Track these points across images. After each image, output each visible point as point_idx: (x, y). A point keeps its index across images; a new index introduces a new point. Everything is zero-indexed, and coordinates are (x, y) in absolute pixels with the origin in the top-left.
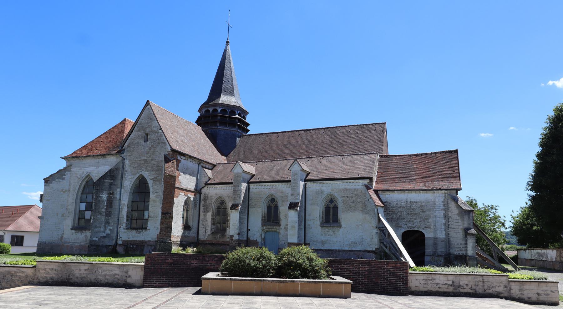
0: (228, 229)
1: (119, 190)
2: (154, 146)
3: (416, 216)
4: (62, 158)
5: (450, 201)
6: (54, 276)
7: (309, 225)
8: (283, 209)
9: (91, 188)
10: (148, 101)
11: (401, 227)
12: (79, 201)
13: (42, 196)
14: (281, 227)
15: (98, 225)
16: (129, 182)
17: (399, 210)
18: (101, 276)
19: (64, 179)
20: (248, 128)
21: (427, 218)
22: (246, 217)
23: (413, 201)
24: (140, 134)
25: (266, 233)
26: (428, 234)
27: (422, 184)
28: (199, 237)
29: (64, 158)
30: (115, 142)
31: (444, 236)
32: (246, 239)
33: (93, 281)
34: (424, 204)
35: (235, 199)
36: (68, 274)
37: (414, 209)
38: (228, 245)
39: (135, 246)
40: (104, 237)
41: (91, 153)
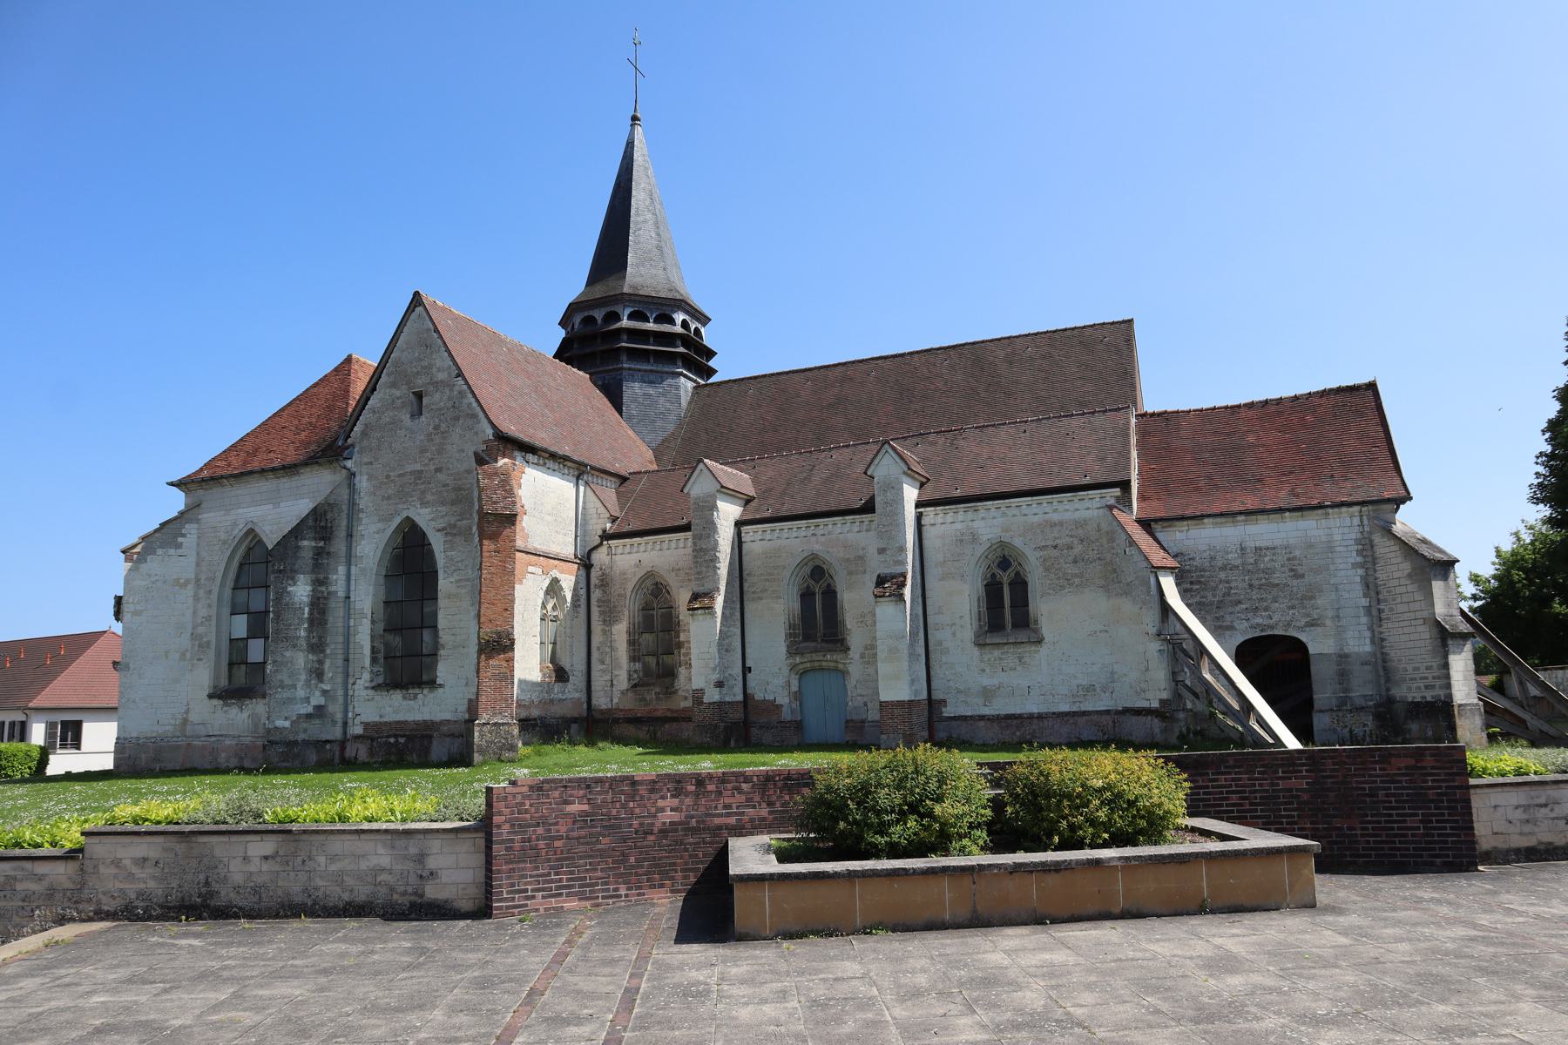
0: (682, 671)
1: (342, 569)
2: (443, 426)
3: (1275, 591)
4: (172, 484)
5: (1377, 538)
6: (152, 884)
7: (940, 643)
8: (854, 598)
9: (258, 566)
10: (417, 294)
11: (1231, 628)
12: (226, 610)
13: (119, 601)
14: (851, 654)
15: (288, 682)
16: (371, 543)
17: (1222, 575)
18: (329, 872)
19: (179, 546)
20: (712, 363)
21: (1310, 595)
22: (738, 631)
23: (1264, 544)
24: (398, 393)
25: (802, 675)
26: (1318, 644)
27: (1283, 494)
28: (594, 702)
29: (178, 484)
30: (322, 429)
31: (1368, 648)
32: (740, 698)
33: (298, 899)
34: (1297, 553)
35: (700, 576)
36: (202, 877)
37: (1268, 572)
38: (689, 719)
39: (402, 740)
40: (309, 716)
41: (255, 465)
